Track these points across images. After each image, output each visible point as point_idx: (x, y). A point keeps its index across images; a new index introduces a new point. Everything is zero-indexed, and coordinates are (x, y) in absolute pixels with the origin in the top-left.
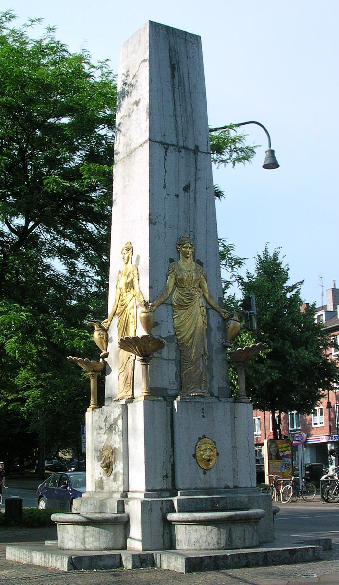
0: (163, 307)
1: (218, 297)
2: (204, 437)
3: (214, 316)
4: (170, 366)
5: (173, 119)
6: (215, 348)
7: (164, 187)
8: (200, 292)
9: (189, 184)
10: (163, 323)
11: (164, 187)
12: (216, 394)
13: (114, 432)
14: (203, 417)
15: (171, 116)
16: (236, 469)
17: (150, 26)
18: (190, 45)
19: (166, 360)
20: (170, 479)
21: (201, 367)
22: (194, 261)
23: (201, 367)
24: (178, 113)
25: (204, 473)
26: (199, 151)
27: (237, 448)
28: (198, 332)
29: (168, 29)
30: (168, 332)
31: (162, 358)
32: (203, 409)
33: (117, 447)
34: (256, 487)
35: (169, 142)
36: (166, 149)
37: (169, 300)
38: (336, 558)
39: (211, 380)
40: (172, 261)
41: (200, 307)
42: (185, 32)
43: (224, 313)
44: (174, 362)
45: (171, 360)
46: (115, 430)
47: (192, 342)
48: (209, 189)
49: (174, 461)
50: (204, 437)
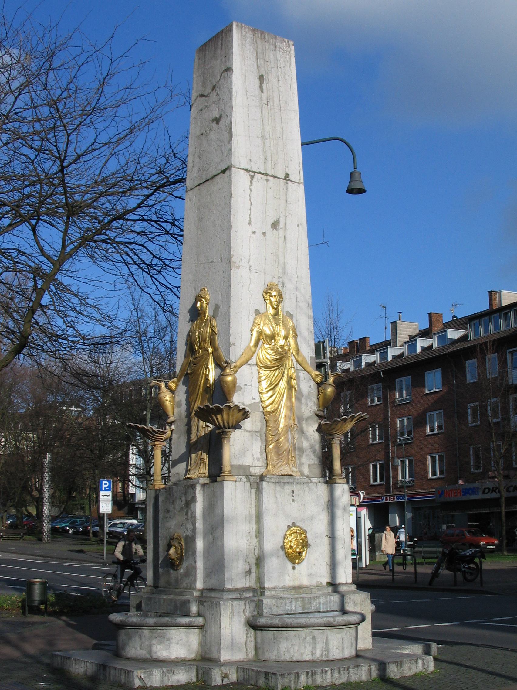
11: (250, 223)
14: (293, 500)
26: (289, 180)
32: (293, 492)
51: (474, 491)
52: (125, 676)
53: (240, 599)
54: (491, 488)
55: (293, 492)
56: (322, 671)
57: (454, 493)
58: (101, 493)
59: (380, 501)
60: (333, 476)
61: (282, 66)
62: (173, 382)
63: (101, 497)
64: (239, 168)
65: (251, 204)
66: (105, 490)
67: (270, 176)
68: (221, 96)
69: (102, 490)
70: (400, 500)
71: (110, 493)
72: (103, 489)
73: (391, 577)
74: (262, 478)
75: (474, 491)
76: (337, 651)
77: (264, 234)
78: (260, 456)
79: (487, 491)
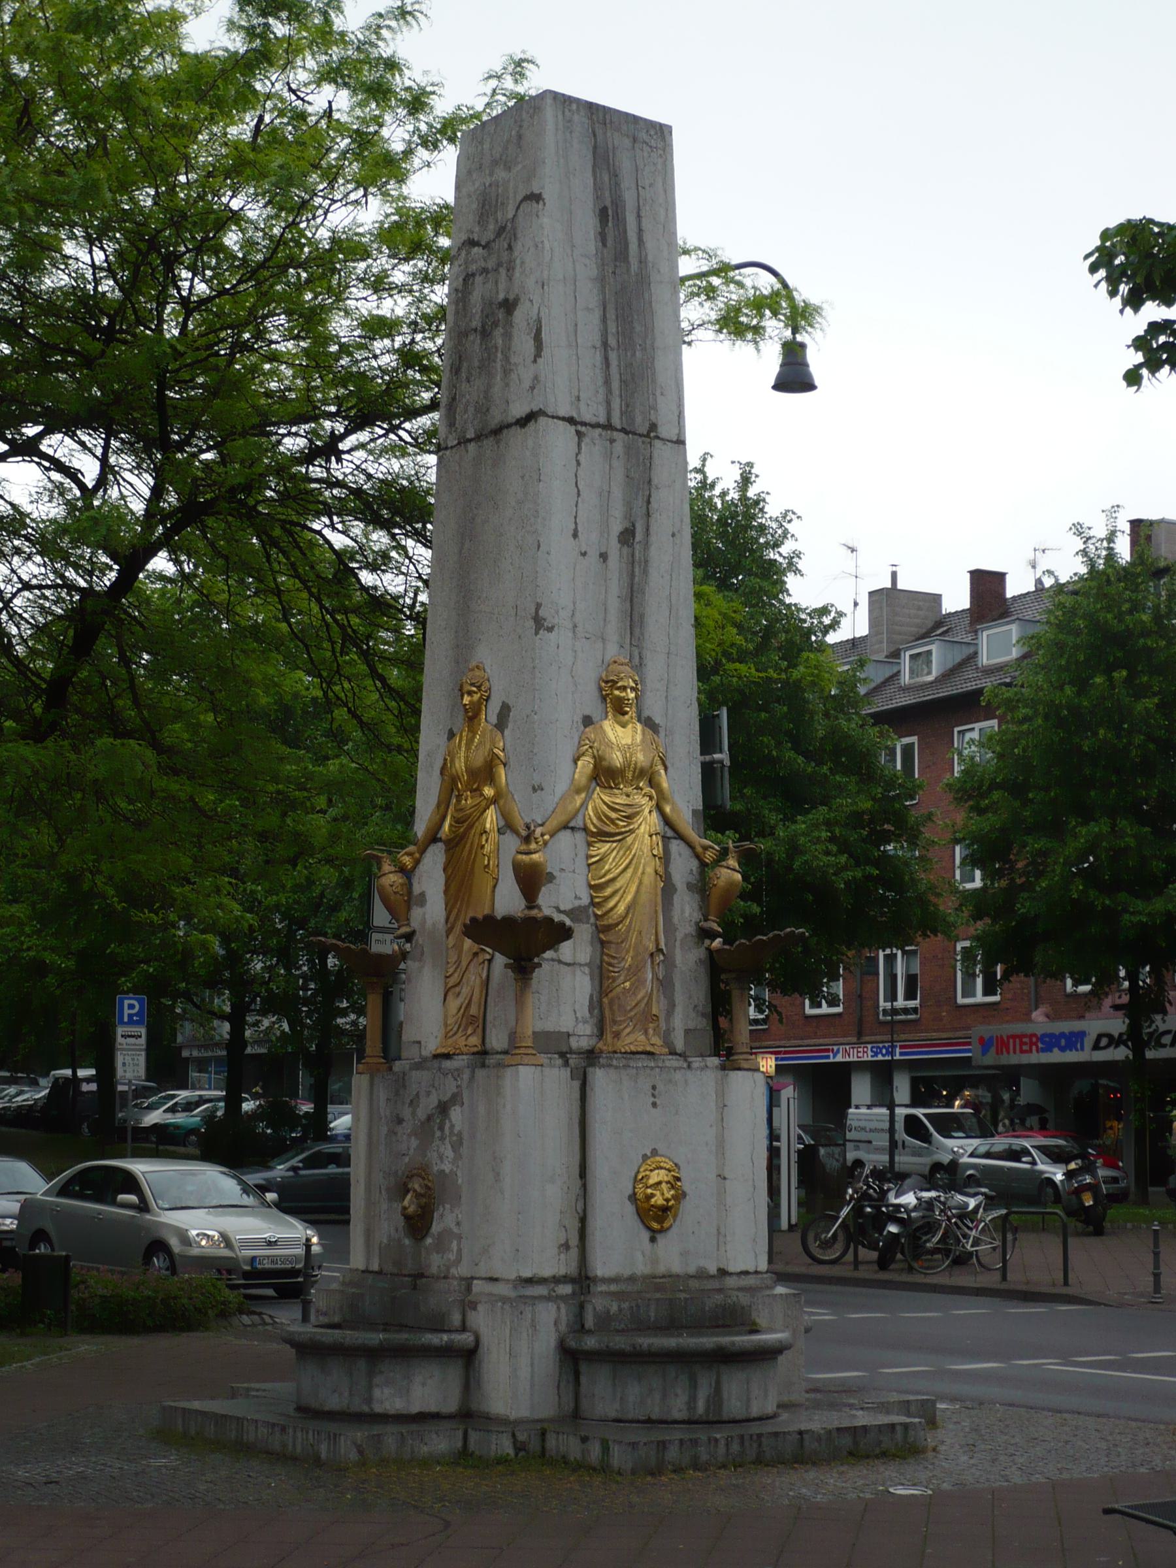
0: (565, 836)
2: (655, 1152)
3: (680, 855)
4: (577, 978)
5: (599, 357)
6: (679, 935)
8: (651, 798)
9: (634, 526)
10: (563, 874)
11: (575, 535)
12: (680, 1045)
13: (438, 1134)
14: (654, 1105)
15: (594, 347)
16: (722, 1230)
17: (809, 376)
18: (646, 154)
19: (568, 965)
20: (574, 1252)
21: (649, 983)
22: (639, 721)
23: (649, 983)
24: (612, 341)
25: (653, 1240)
26: (658, 437)
27: (725, 1178)
28: (644, 897)
29: (592, 108)
30: (576, 897)
32: (654, 1088)
33: (447, 1171)
34: (767, 1272)
35: (587, 417)
37: (580, 817)
39: (670, 1012)
40: (588, 721)
41: (651, 836)
42: (634, 116)
43: (705, 848)
44: (587, 970)
45: (581, 965)
46: (441, 1128)
47: (630, 923)
49: (585, 1210)
50: (655, 1152)
51: (1073, 1040)
52: (329, 1444)
53: (548, 1298)
54: (1116, 1035)
55: (654, 1088)
56: (709, 1439)
57: (1022, 1044)
58: (120, 1030)
59: (828, 1057)
60: (733, 1055)
61: (647, 182)
62: (409, 854)
63: (119, 1039)
64: (553, 417)
65: (579, 495)
66: (131, 1022)
67: (617, 430)
68: (516, 253)
69: (122, 1022)
70: (880, 1057)
71: (143, 1031)
72: (126, 1019)
73: (886, 1158)
74: (591, 1056)
75: (1073, 1040)
76: (738, 1404)
77: (604, 556)
78: (588, 1015)
79: (1104, 1041)
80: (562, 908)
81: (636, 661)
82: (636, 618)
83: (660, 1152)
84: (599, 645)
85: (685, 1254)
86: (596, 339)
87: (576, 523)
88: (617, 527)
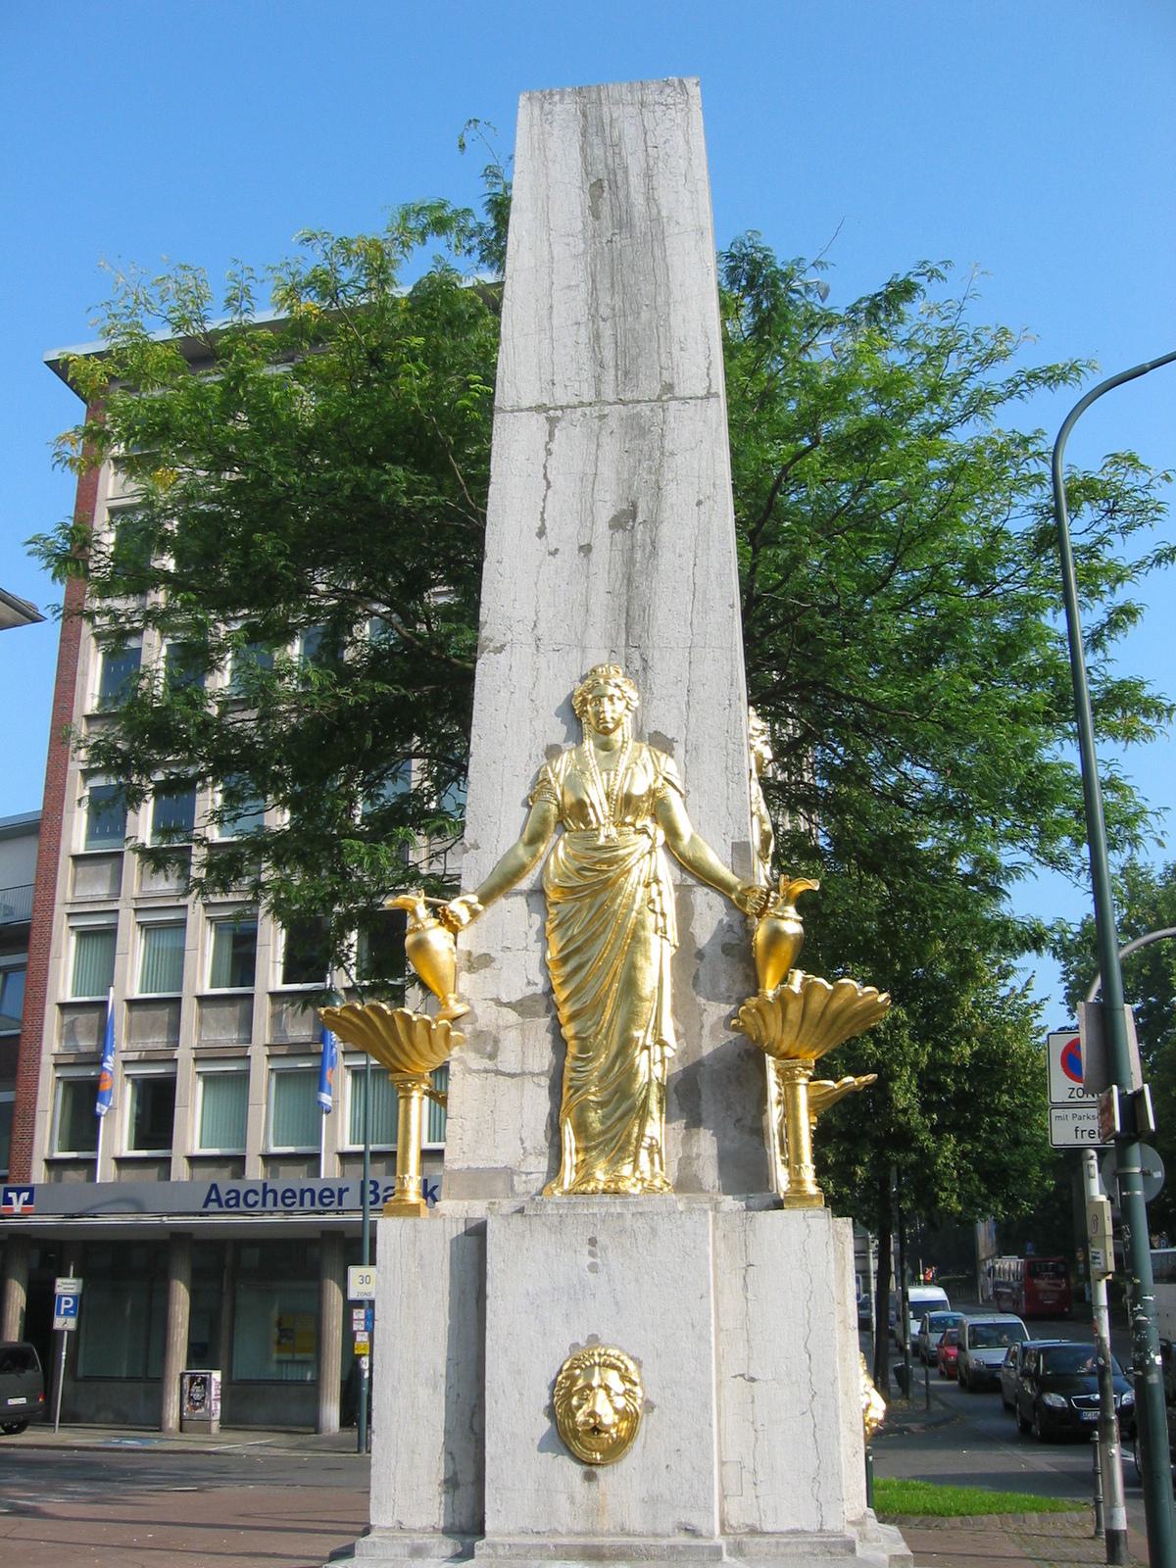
1: (730, 842)
3: (711, 908)
7: (541, 533)
11: (541, 533)
19: (512, 1076)
25: (590, 1477)
31: (498, 1072)
32: (593, 1242)
36: (552, 422)
38: (3, 1349)
45: (533, 1074)
48: (708, 504)
55: (593, 1242)
65: (549, 486)
77: (586, 549)
80: (505, 1000)
81: (637, 664)
82: (636, 612)
83: (603, 1340)
84: (576, 654)
85: (652, 1501)
86: (582, 312)
87: (543, 520)
88: (605, 514)
